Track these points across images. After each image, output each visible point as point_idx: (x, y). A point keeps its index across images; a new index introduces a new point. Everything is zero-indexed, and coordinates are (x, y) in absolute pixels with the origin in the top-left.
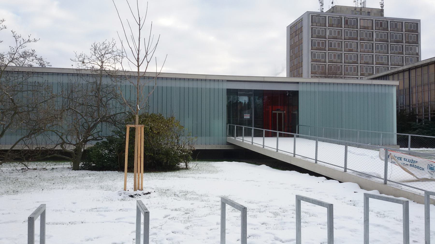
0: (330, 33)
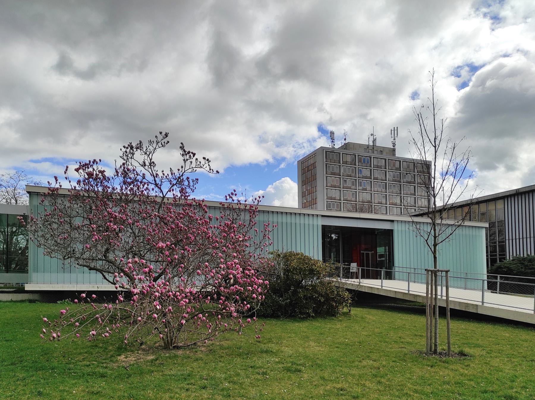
0: (345, 171)
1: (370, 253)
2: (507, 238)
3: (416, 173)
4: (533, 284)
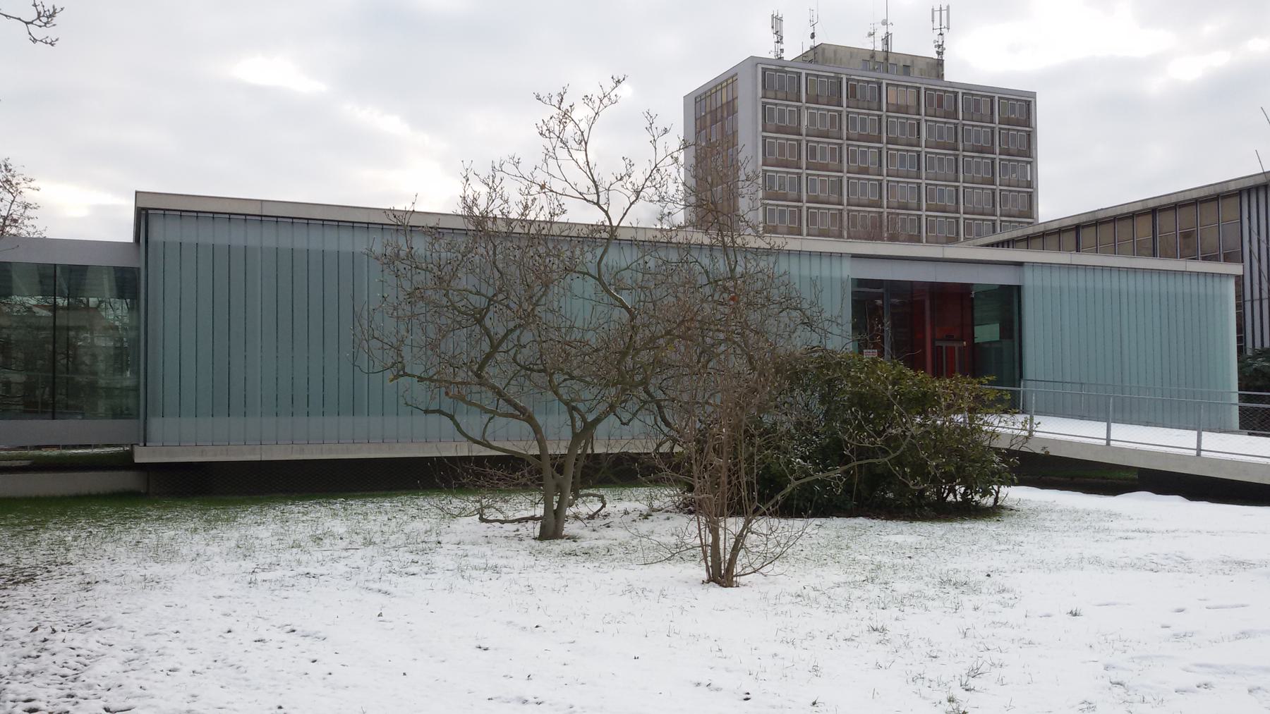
1: (956, 345)
2: (952, 252)
3: (997, 126)
4: (1267, 406)
